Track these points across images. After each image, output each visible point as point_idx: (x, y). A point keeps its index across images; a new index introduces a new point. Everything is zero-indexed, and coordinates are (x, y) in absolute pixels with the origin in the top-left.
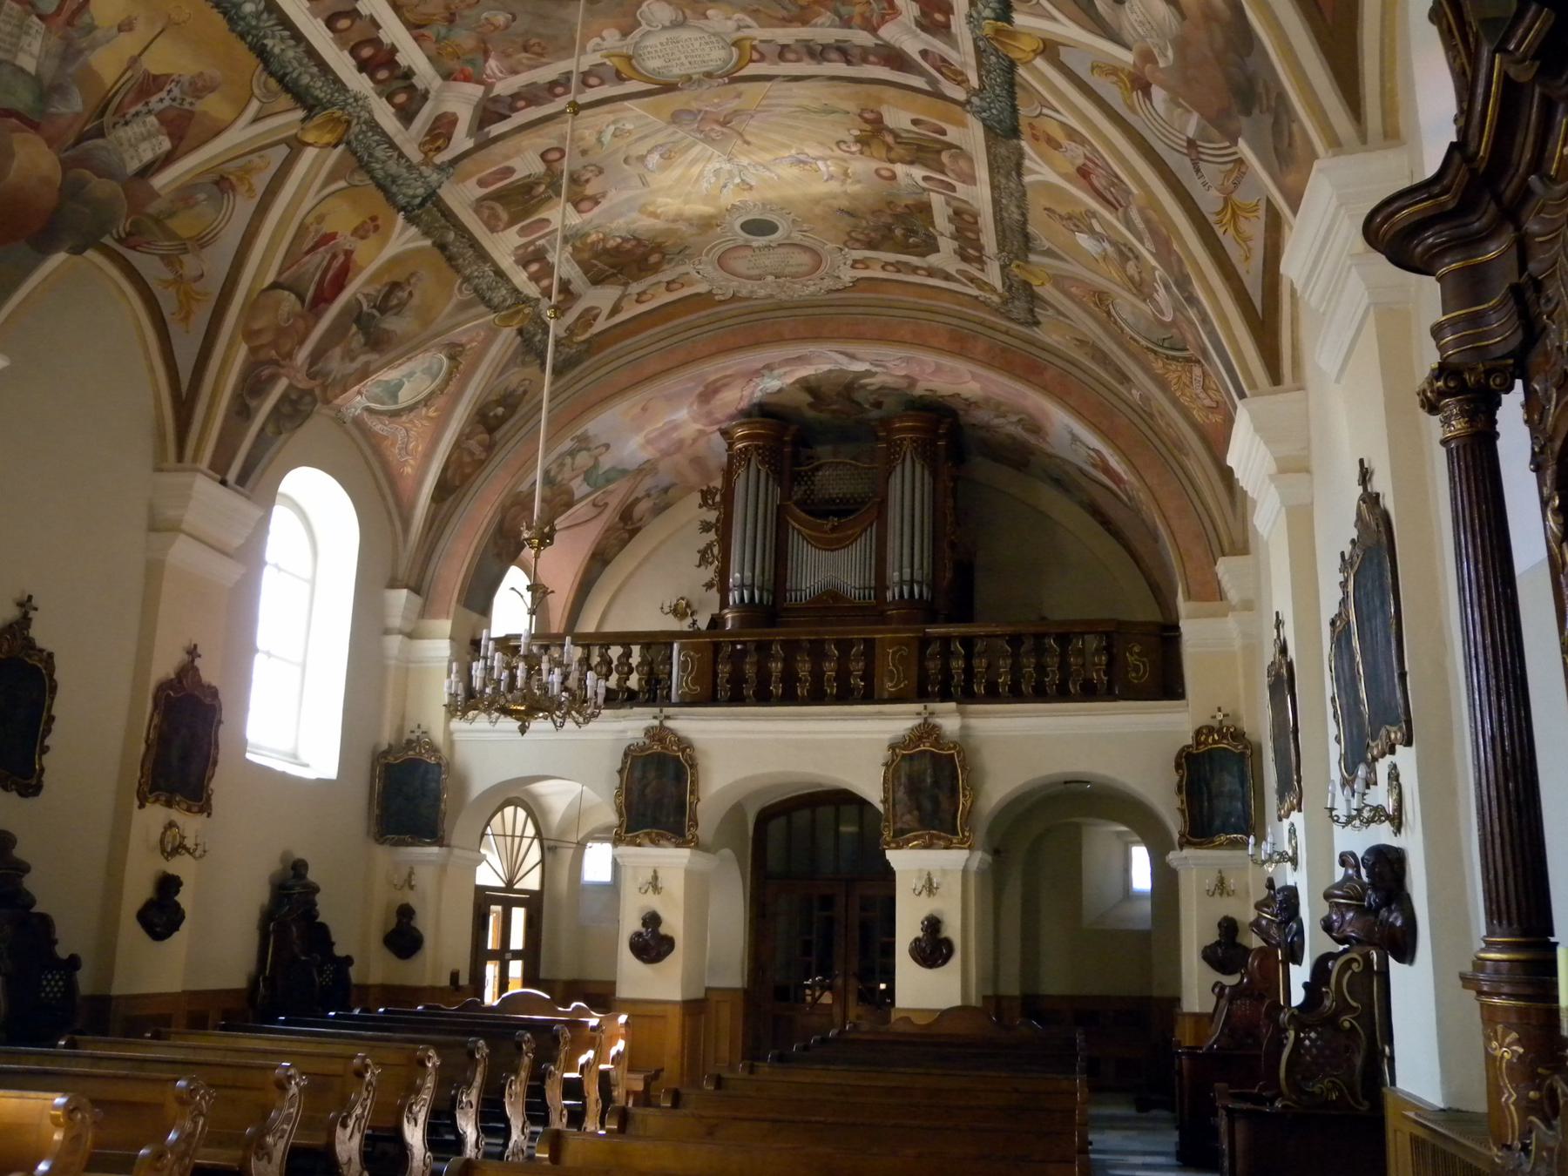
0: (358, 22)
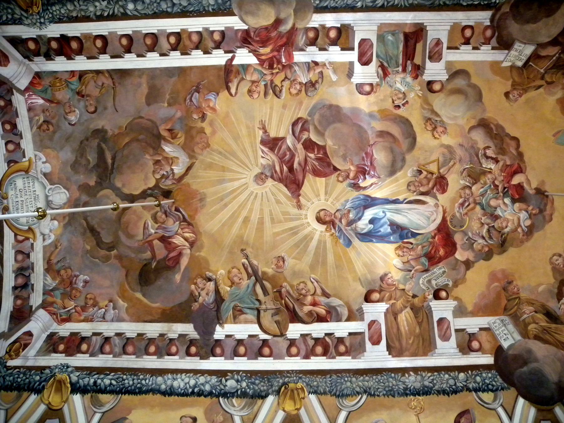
0: (170, 47)
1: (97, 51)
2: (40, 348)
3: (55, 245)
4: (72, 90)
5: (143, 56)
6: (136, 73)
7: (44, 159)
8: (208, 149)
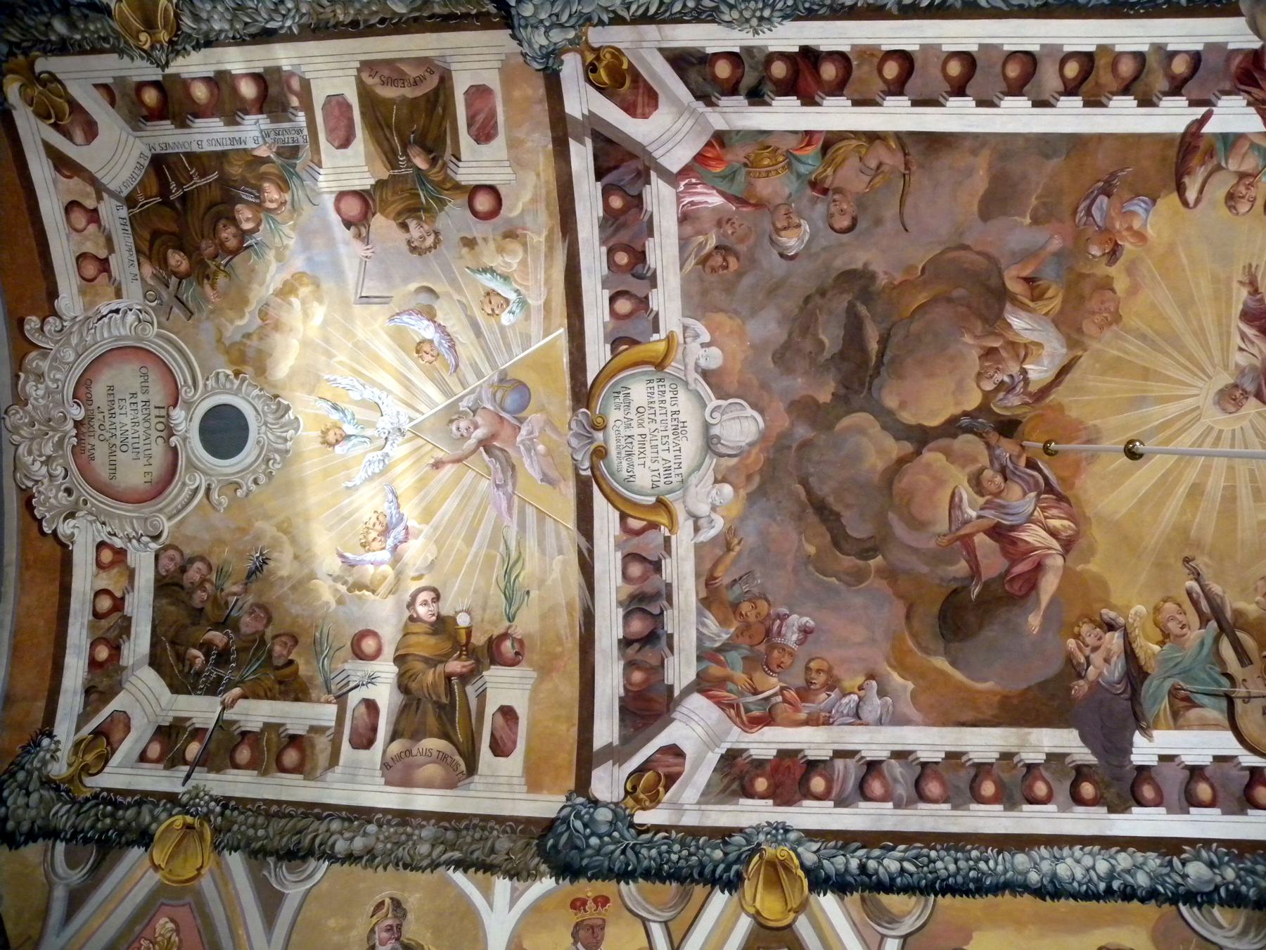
0: (1061, 88)
1: (882, 86)
2: (708, 785)
3: (726, 542)
4: (799, 176)
5: (991, 104)
6: (967, 143)
7: (706, 337)
8: (1114, 327)
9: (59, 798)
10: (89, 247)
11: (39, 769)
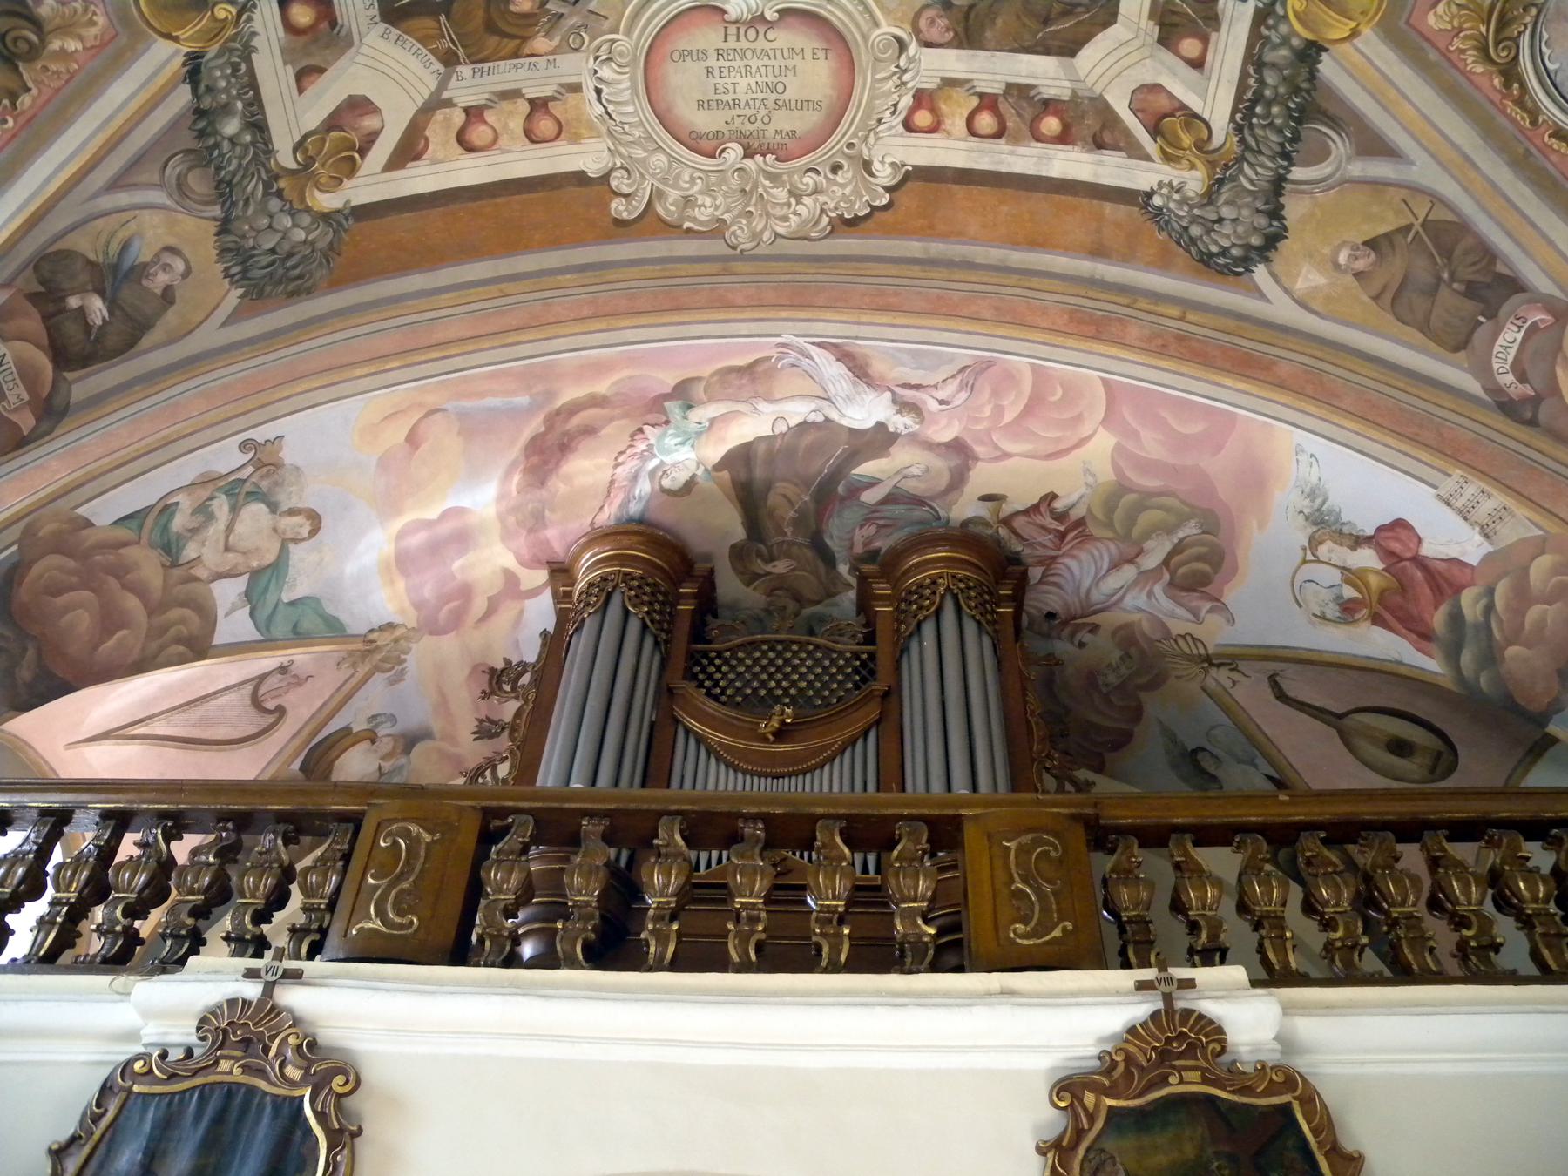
9: (1233, 179)
10: (517, 124)
11: (1191, 207)
